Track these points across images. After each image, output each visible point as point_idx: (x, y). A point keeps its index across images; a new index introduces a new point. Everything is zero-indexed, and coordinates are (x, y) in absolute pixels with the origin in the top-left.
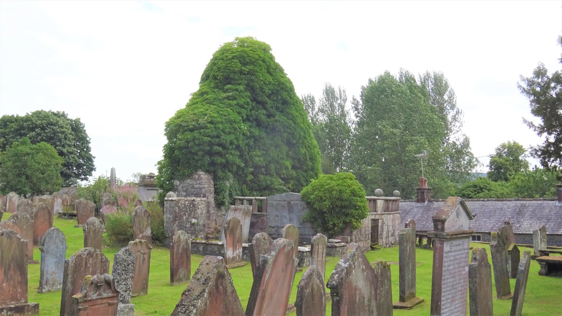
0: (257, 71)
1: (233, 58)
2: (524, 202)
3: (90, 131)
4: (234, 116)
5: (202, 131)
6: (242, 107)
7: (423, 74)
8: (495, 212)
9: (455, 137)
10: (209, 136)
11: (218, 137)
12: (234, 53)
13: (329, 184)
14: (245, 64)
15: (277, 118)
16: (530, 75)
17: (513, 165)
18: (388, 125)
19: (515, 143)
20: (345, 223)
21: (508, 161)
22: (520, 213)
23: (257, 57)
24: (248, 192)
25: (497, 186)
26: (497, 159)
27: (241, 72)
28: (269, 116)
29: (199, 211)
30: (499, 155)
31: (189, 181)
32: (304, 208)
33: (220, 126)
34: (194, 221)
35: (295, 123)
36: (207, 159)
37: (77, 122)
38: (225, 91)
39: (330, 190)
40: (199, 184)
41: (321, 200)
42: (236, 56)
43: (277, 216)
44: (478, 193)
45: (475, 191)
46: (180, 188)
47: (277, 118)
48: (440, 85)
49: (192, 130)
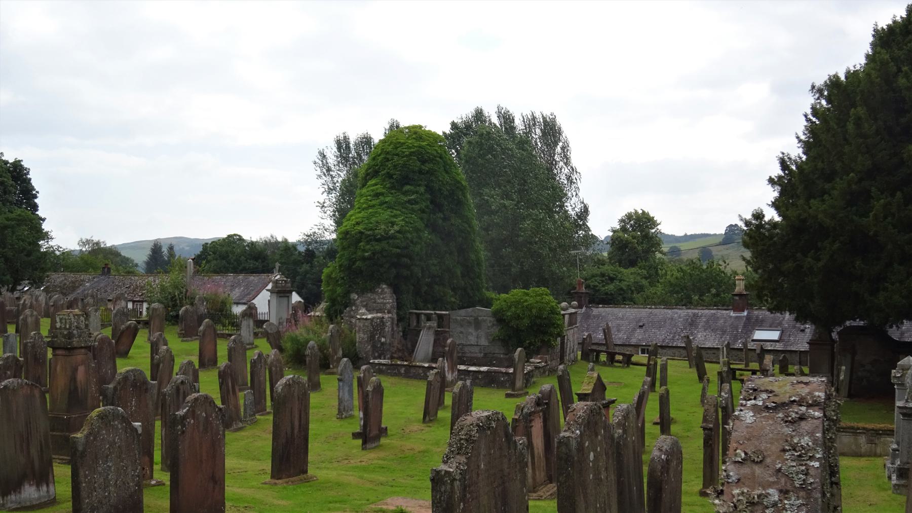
0: (436, 171)
1: (411, 154)
2: (696, 311)
3: (37, 180)
4: (420, 224)
5: (391, 241)
6: (423, 211)
7: (527, 113)
8: (665, 322)
9: (572, 207)
10: (398, 247)
11: (406, 248)
12: (410, 148)
13: (526, 301)
14: (423, 162)
15: (453, 221)
16: (748, 216)
17: (642, 243)
18: (497, 195)
19: (644, 212)
20: (543, 341)
21: (634, 238)
22: (692, 323)
23: (435, 153)
24: (421, 304)
25: (630, 275)
26: (621, 234)
27: (420, 172)
28: (445, 219)
29: (387, 329)
30: (624, 229)
31: (369, 295)
32: (493, 325)
33: (409, 236)
34: (383, 340)
35: (470, 227)
36: (394, 271)
37: (17, 165)
38: (405, 193)
39: (530, 308)
40: (383, 298)
41: (518, 317)
42: (413, 152)
43: (461, 332)
44: (608, 284)
45: (603, 281)
46: (358, 302)
47: (453, 221)
48: (551, 131)
49: (378, 240)
